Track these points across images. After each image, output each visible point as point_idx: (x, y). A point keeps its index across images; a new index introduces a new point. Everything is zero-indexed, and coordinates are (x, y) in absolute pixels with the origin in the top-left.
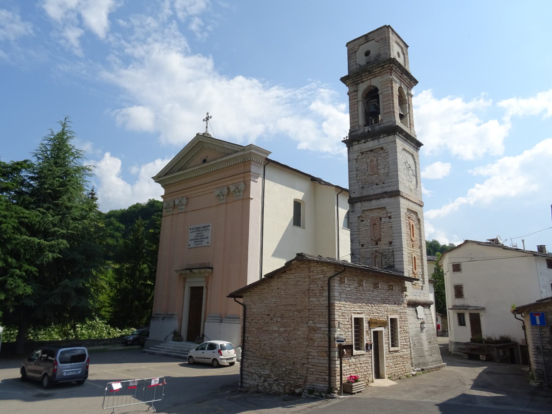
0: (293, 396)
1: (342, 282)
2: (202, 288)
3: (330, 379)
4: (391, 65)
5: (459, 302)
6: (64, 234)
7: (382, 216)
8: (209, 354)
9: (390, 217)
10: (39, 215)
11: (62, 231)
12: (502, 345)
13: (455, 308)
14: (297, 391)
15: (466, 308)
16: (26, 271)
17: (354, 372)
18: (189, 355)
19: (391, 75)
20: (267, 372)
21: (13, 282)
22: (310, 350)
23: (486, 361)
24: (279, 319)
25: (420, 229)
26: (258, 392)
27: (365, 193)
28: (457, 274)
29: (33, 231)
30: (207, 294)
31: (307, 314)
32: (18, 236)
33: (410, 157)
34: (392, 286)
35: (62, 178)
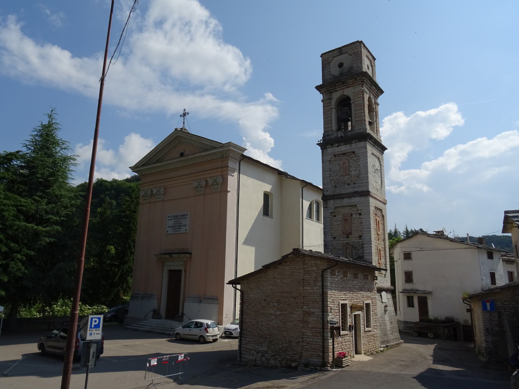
0: (290, 369)
1: (332, 274)
2: (181, 271)
3: (323, 355)
4: (363, 78)
5: (409, 286)
6: (57, 221)
7: (353, 213)
8: (196, 332)
9: (360, 214)
10: (34, 204)
11: (55, 218)
12: (447, 324)
13: (404, 291)
14: (293, 365)
15: (415, 291)
16: (27, 255)
17: (341, 349)
18: (176, 332)
19: (362, 87)
20: (265, 349)
21: (14, 266)
22: (305, 331)
23: (433, 338)
24: (276, 304)
25: (384, 224)
26: (256, 365)
27: (337, 192)
28: (408, 262)
29: (29, 218)
30: (185, 277)
31: (302, 300)
32: (17, 223)
33: (377, 160)
34: (367, 275)
35: (53, 169)
